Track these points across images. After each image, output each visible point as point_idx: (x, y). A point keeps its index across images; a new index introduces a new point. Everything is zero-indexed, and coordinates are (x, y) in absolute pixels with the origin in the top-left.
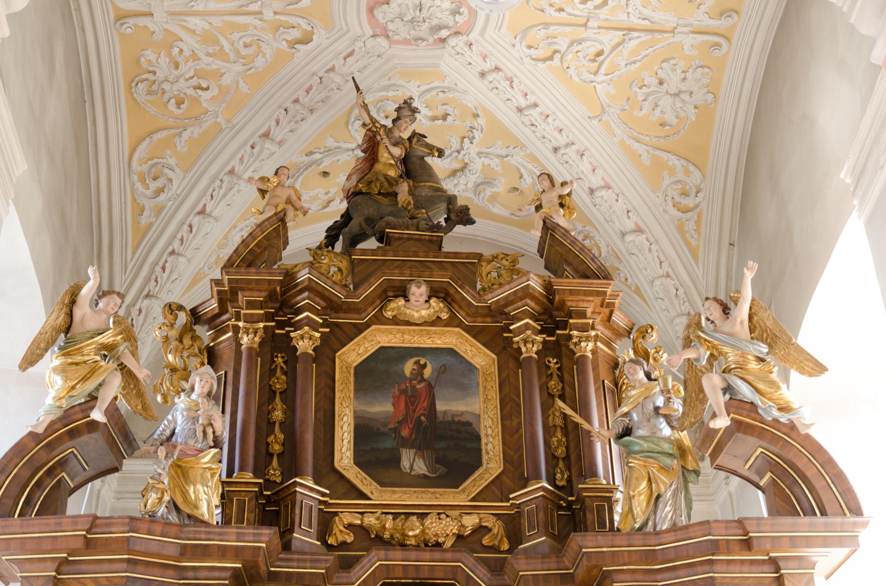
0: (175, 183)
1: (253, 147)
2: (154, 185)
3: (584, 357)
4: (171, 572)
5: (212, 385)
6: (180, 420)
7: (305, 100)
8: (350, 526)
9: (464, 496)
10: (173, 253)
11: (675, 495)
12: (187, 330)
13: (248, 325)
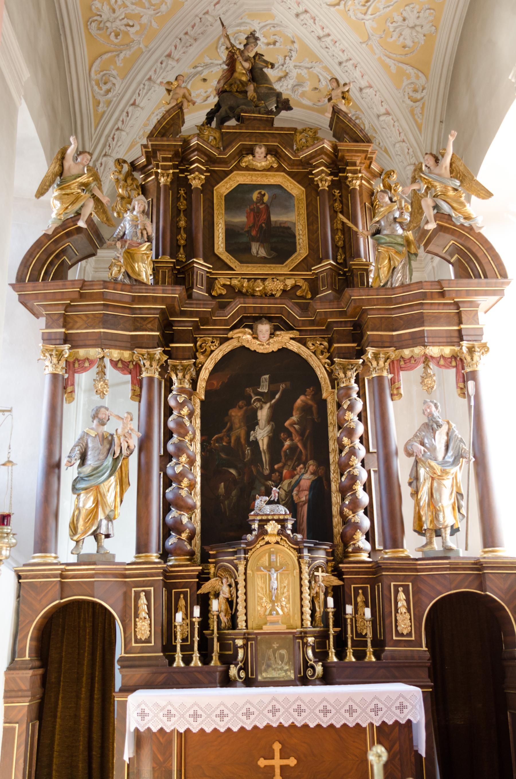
0: (117, 86)
1: (161, 63)
2: (105, 88)
3: (354, 189)
4: (127, 311)
5: (145, 206)
6: (128, 226)
7: (192, 33)
8: (224, 285)
9: (286, 269)
10: (118, 129)
11: (403, 267)
12: (129, 175)
13: (164, 172)
